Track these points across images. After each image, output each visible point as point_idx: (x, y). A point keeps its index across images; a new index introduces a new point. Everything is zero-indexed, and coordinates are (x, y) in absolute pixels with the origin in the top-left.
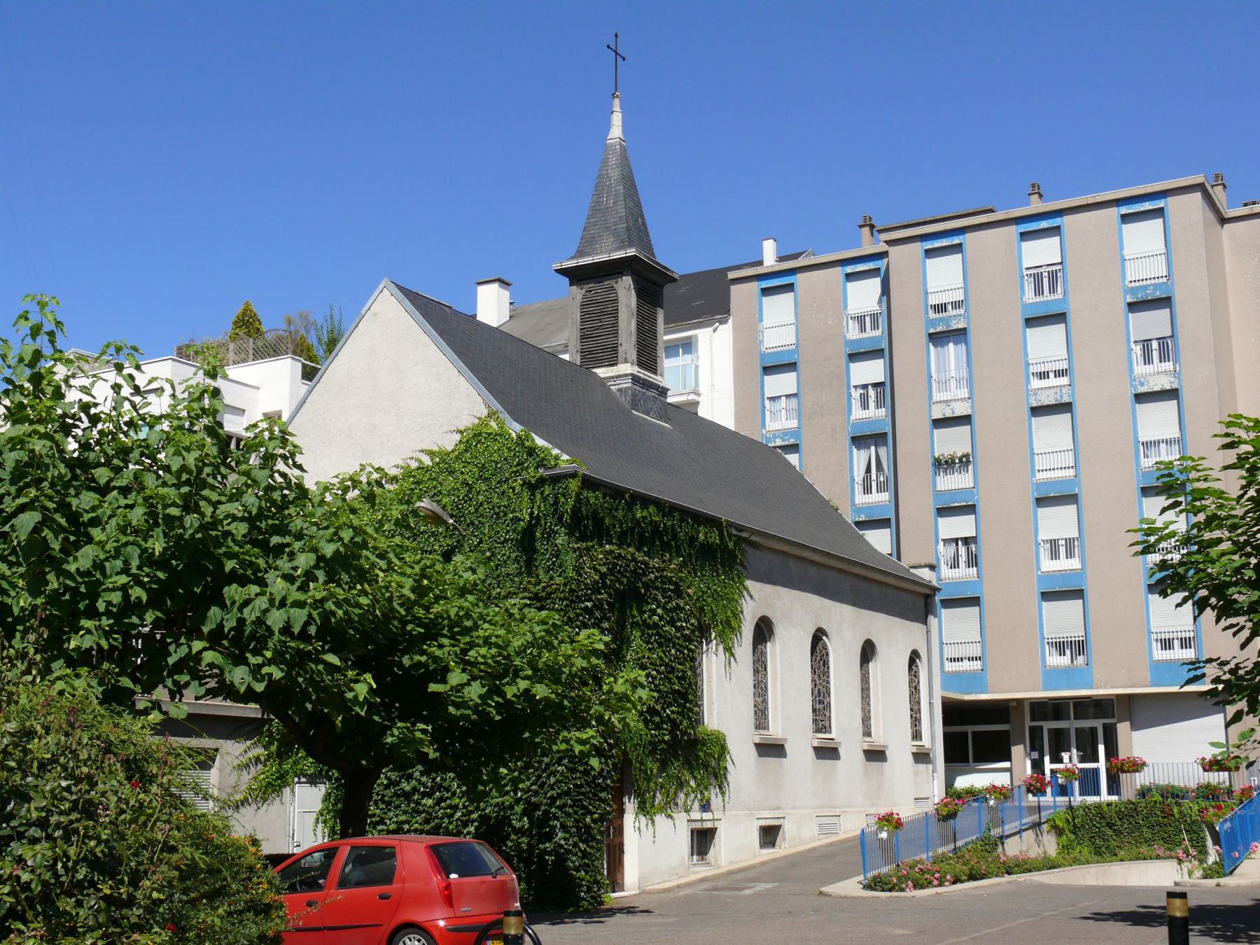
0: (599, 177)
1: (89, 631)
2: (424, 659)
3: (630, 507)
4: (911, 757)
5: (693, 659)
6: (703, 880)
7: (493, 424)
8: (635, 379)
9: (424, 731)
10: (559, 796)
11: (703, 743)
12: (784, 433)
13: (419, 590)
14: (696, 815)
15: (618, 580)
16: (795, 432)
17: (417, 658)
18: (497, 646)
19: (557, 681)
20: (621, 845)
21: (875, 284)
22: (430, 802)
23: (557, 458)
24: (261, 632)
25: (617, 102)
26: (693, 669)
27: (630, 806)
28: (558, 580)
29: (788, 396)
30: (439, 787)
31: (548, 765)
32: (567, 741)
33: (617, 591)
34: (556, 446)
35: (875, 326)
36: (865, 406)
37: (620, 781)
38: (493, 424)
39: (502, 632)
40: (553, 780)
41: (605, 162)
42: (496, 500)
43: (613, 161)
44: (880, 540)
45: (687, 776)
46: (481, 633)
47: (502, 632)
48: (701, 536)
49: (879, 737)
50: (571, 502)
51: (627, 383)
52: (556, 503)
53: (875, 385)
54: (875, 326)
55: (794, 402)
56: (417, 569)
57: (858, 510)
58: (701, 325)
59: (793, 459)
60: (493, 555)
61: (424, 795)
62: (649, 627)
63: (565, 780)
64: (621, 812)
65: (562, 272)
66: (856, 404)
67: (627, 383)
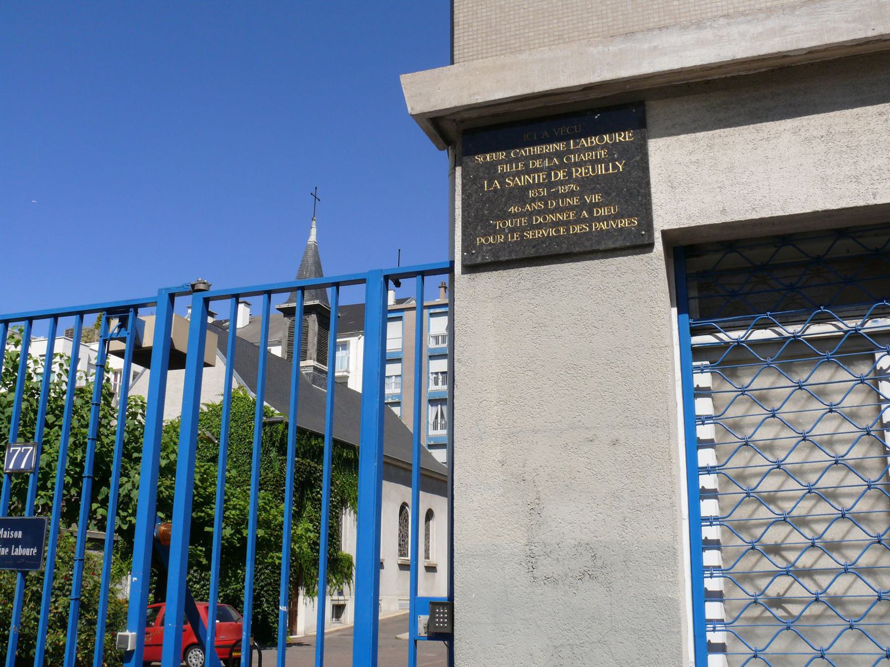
0: (302, 261)
1: (42, 497)
2: (203, 514)
3: (309, 439)
4: (397, 567)
5: (338, 518)
6: (337, 631)
7: (241, 393)
8: (315, 368)
9: (201, 551)
10: (266, 585)
11: (341, 560)
12: (393, 396)
13: (203, 480)
14: (335, 597)
15: (301, 476)
16: (399, 396)
17: (200, 514)
18: (239, 509)
19: (269, 527)
20: (296, 611)
21: (444, 320)
22: (198, 586)
23: (273, 412)
24: (126, 500)
25: (314, 222)
26: (337, 522)
27: (302, 592)
28: (270, 475)
29: (396, 376)
30: (203, 579)
31: (261, 569)
32: (272, 558)
33: (300, 482)
34: (273, 406)
35: (444, 342)
36: (436, 384)
37: (297, 579)
38: (241, 393)
39: (242, 503)
40: (263, 577)
41: (306, 253)
42: (240, 432)
43: (310, 253)
44: (440, 456)
45: (332, 577)
46: (232, 503)
47: (242, 503)
48: (345, 454)
49: (433, 559)
50: (280, 436)
51: (311, 370)
52: (272, 435)
53: (442, 373)
54: (444, 342)
55: (399, 379)
56: (202, 470)
57: (430, 438)
58: (352, 335)
59: (396, 410)
60: (238, 460)
61: (195, 583)
62: (316, 500)
63: (269, 577)
64: (297, 595)
65: (279, 309)
66: (431, 382)
67: (311, 370)
